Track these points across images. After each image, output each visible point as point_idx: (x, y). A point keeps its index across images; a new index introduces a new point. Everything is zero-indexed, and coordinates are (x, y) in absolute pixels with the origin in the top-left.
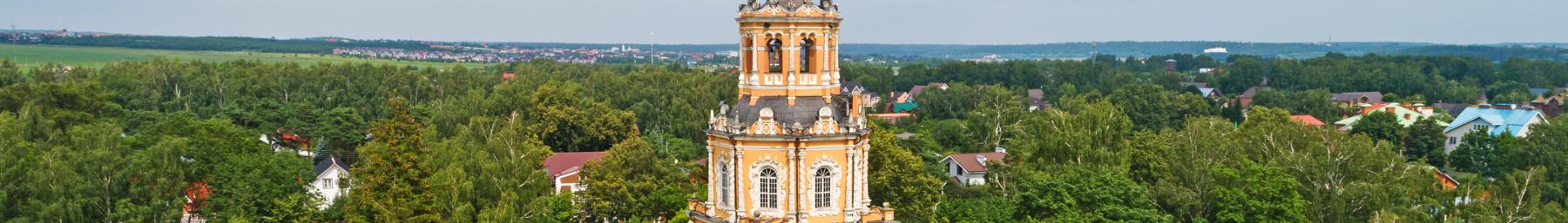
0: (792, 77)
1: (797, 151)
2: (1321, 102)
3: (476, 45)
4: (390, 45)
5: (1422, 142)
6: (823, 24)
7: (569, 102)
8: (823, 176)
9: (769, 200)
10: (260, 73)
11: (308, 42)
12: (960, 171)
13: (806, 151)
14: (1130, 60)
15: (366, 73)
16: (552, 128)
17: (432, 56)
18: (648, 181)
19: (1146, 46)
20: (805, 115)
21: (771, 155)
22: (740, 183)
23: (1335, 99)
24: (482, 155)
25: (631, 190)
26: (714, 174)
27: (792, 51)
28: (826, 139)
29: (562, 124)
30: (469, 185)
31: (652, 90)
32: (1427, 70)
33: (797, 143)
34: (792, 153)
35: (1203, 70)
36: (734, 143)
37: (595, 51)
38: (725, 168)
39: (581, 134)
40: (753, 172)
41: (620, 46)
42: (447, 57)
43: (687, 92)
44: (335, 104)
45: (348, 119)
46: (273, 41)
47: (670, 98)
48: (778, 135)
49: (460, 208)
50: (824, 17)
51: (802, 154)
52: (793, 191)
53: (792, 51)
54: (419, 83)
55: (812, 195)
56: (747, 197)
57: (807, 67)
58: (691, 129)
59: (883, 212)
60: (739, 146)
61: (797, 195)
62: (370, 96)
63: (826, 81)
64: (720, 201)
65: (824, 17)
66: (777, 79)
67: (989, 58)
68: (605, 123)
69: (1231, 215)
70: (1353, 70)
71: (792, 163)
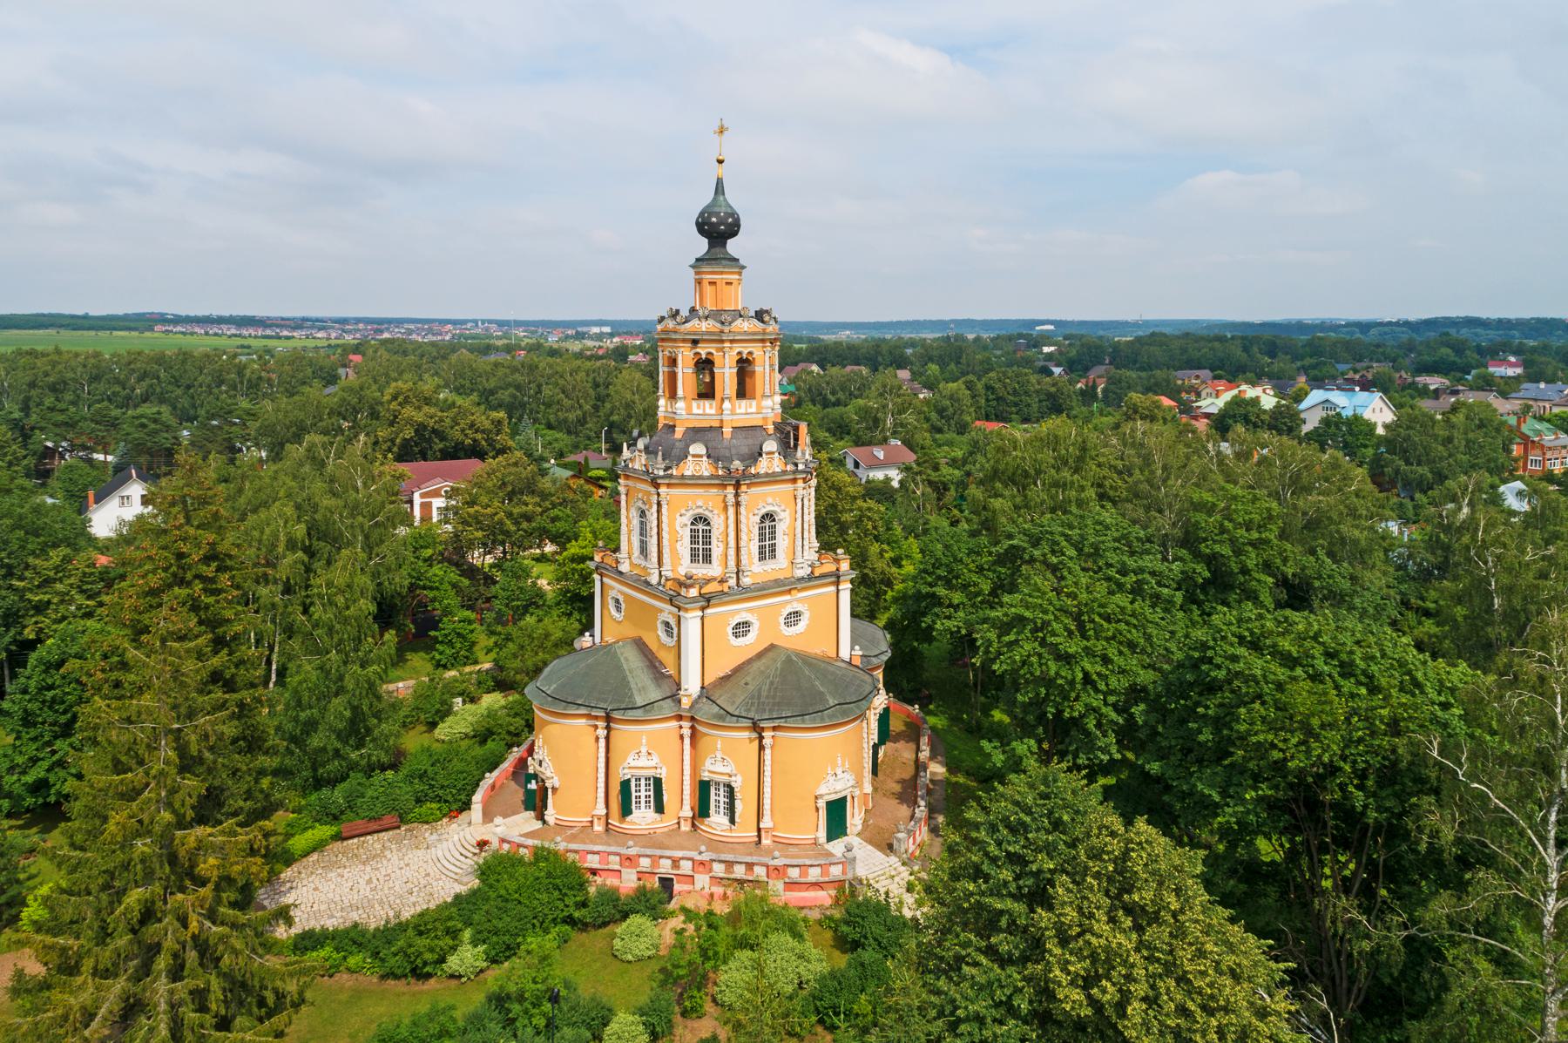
0: (727, 405)
1: (737, 495)
2: (1168, 381)
3: (317, 320)
4: (221, 320)
5: (1284, 422)
6: (763, 341)
7: (428, 401)
8: (767, 524)
9: (702, 554)
10: (54, 364)
11: (126, 317)
12: (857, 465)
13: (749, 495)
14: (978, 339)
15: (184, 362)
16: (409, 433)
17: (268, 332)
18: (531, 504)
19: (986, 324)
20: (745, 450)
21: (706, 501)
22: (665, 535)
23: (1189, 378)
24: (319, 486)
25: (510, 515)
26: (628, 520)
27: (726, 374)
28: (772, 479)
29: (420, 429)
30: (300, 530)
31: (518, 377)
32: (1246, 349)
33: (737, 486)
34: (731, 499)
35: (1046, 349)
36: (657, 486)
37: (450, 327)
38: (643, 514)
39: (443, 438)
40: (679, 521)
41: (476, 322)
42: (285, 333)
43: (561, 382)
44: (145, 399)
45: (155, 421)
46: (86, 317)
47: (539, 386)
48: (712, 477)
49: (290, 558)
50: (764, 333)
51: (743, 498)
52: (732, 543)
53: (726, 374)
54: (248, 372)
55: (754, 547)
56: (674, 551)
57: (742, 393)
58: (565, 420)
59: (837, 561)
60: (663, 490)
61: (738, 549)
62: (188, 387)
63: (766, 407)
64: (636, 552)
65: (764, 333)
66: (708, 407)
67: (844, 335)
68: (472, 425)
69: (1217, 548)
70: (1184, 350)
71: (731, 511)
